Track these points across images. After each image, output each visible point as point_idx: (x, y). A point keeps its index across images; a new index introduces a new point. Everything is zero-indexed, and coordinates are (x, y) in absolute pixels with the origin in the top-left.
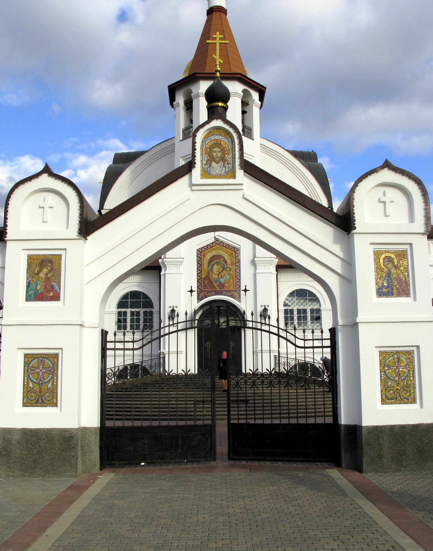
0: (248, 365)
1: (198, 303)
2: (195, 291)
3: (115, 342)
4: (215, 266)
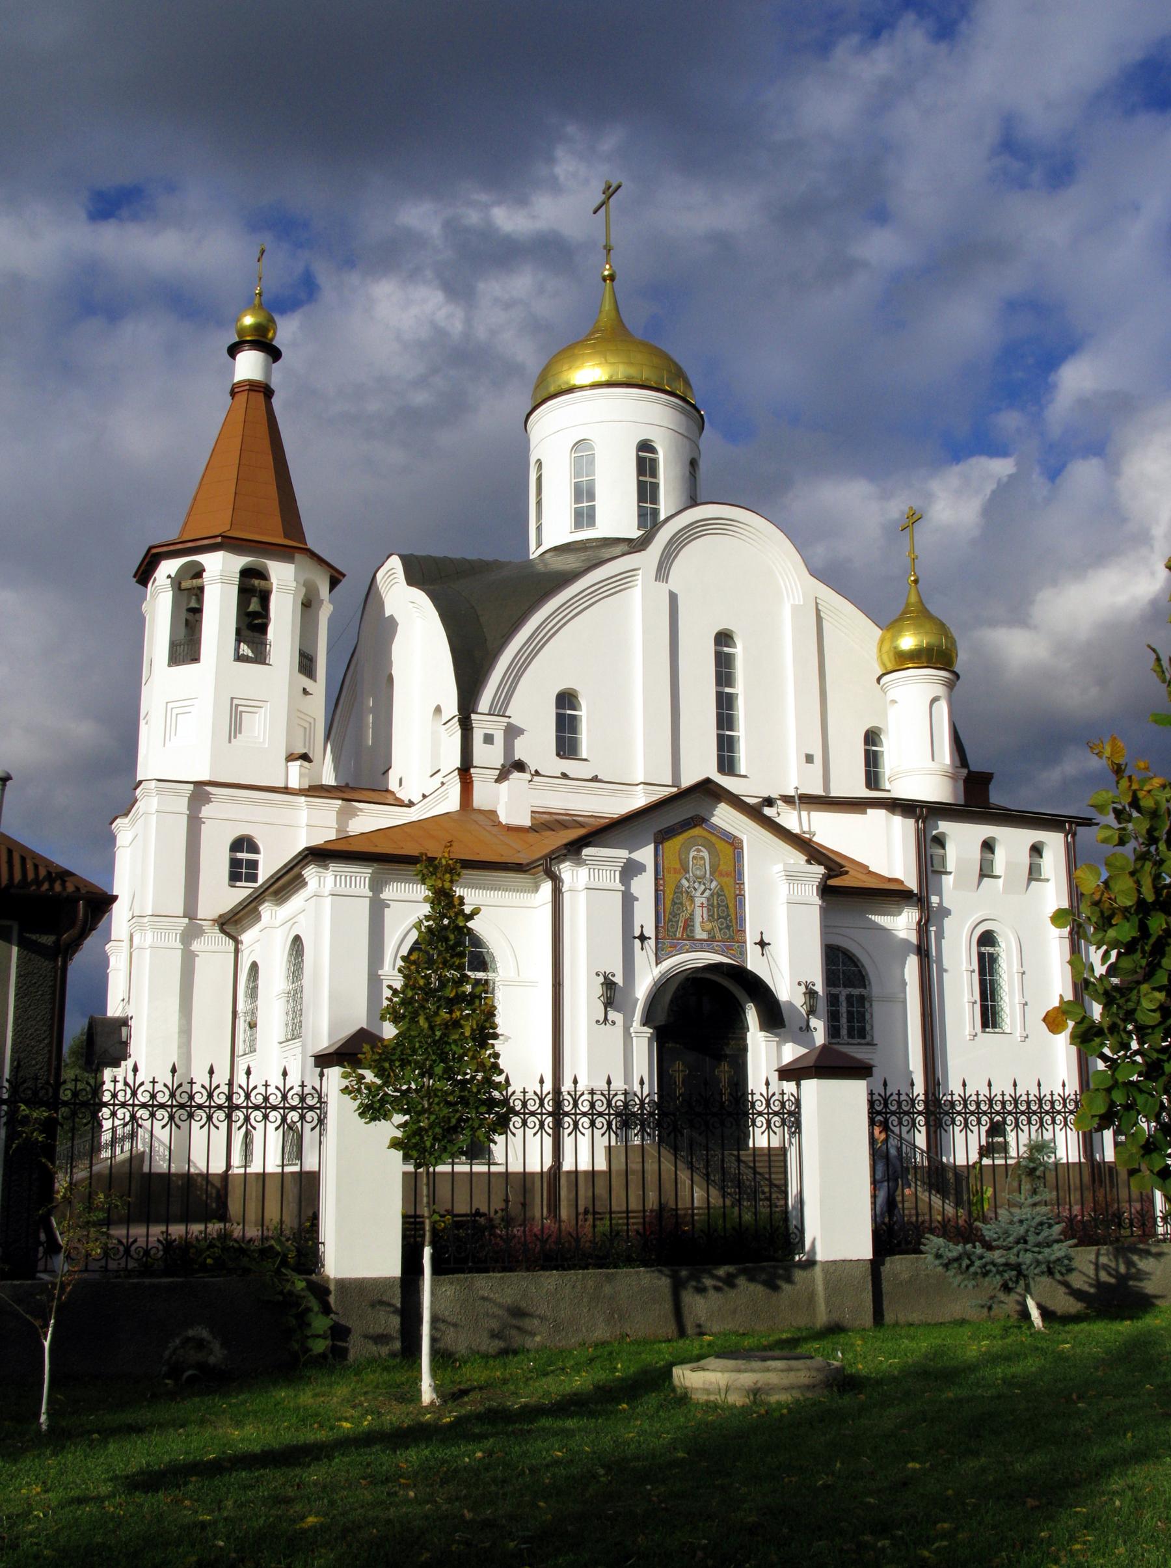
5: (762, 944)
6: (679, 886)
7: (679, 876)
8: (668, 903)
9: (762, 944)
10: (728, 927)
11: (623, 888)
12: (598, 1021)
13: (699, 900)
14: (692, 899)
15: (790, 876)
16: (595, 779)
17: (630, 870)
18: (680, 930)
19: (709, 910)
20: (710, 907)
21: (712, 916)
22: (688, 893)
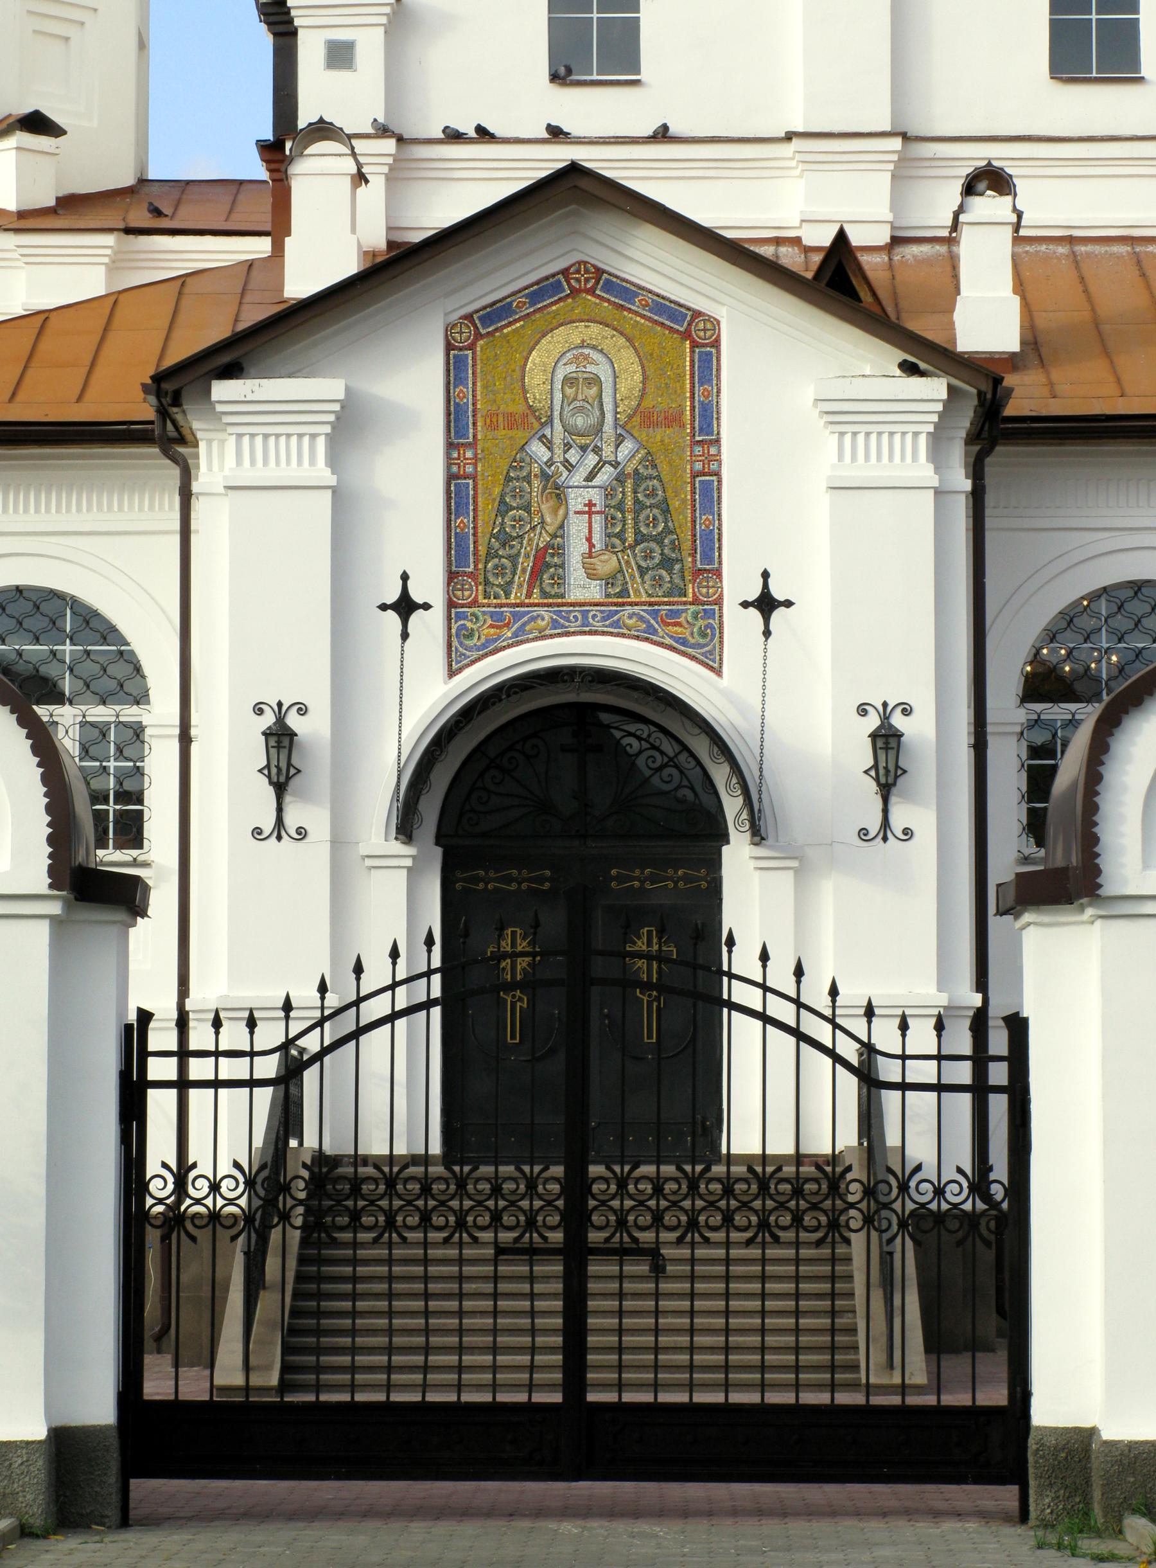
0: (743, 1136)
1: (452, 673)
2: (426, 606)
3: (217, 1054)
4: (548, 455)
5: (766, 604)
6: (519, 460)
7: (520, 435)
8: (487, 509)
9: (766, 604)
10: (667, 563)
11: (332, 481)
12: (257, 832)
13: (576, 500)
14: (559, 494)
15: (839, 415)
16: (662, 135)
17: (349, 427)
18: (522, 578)
19: (610, 520)
20: (613, 510)
21: (620, 535)
22: (545, 477)
